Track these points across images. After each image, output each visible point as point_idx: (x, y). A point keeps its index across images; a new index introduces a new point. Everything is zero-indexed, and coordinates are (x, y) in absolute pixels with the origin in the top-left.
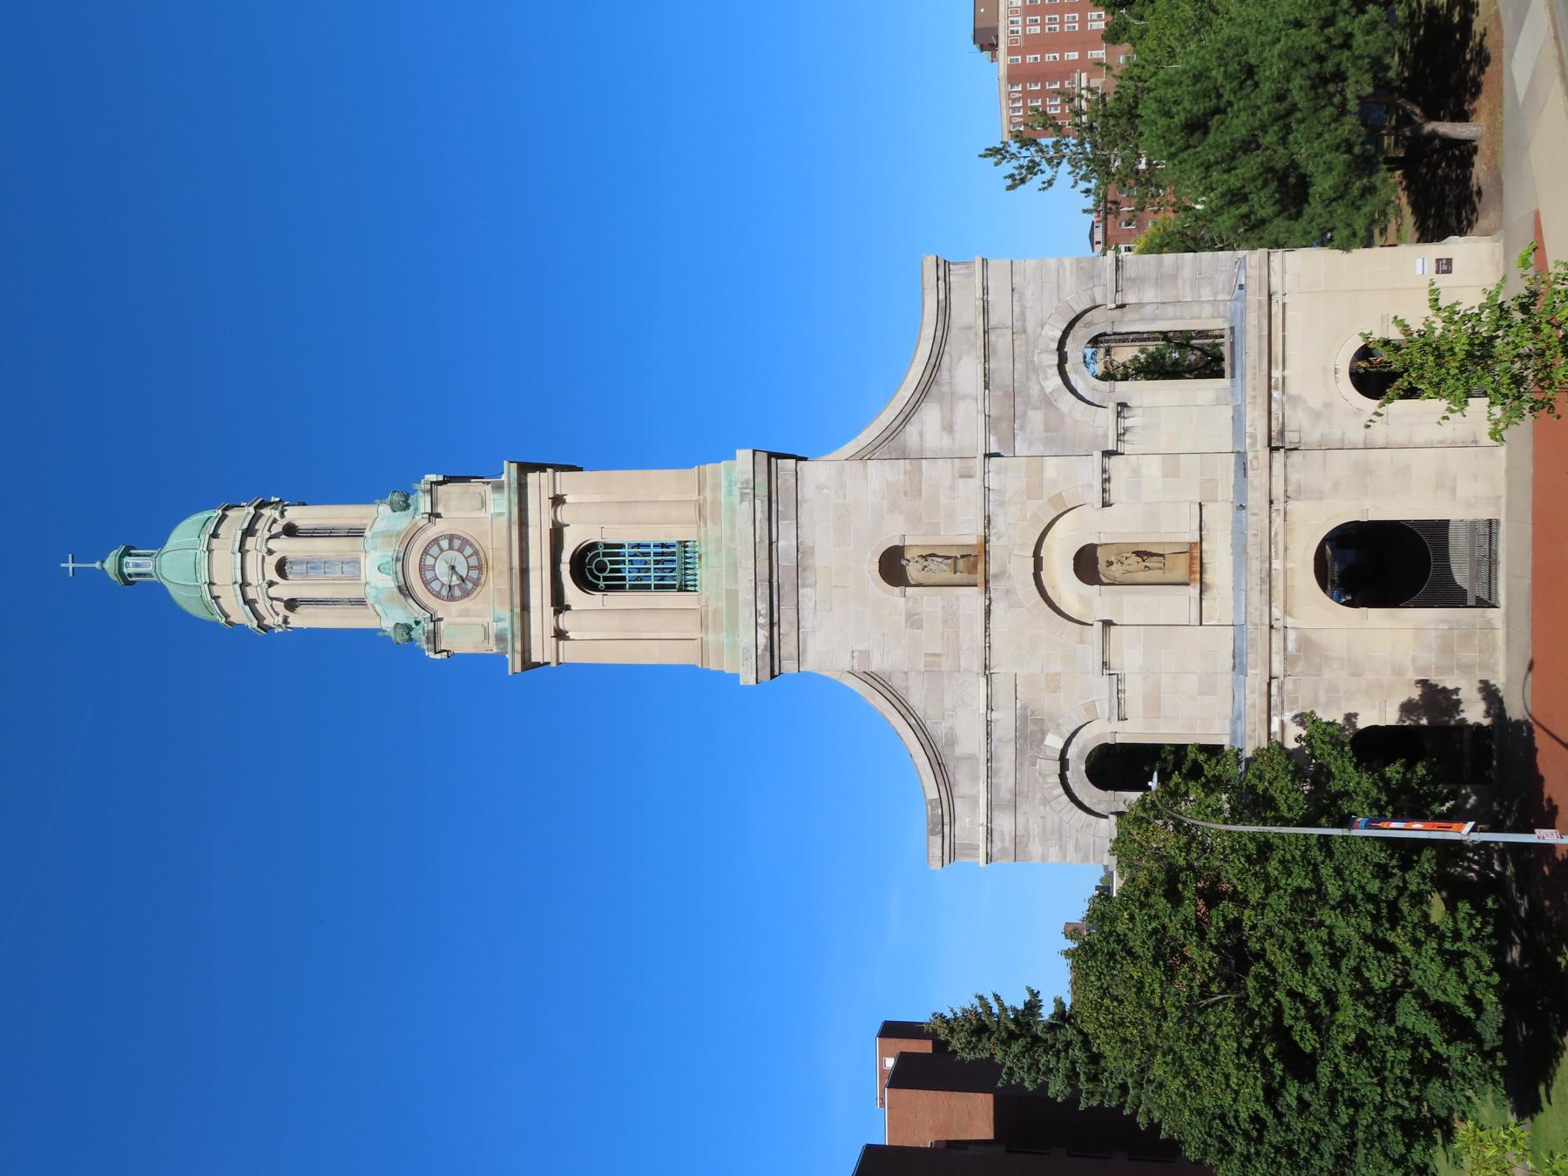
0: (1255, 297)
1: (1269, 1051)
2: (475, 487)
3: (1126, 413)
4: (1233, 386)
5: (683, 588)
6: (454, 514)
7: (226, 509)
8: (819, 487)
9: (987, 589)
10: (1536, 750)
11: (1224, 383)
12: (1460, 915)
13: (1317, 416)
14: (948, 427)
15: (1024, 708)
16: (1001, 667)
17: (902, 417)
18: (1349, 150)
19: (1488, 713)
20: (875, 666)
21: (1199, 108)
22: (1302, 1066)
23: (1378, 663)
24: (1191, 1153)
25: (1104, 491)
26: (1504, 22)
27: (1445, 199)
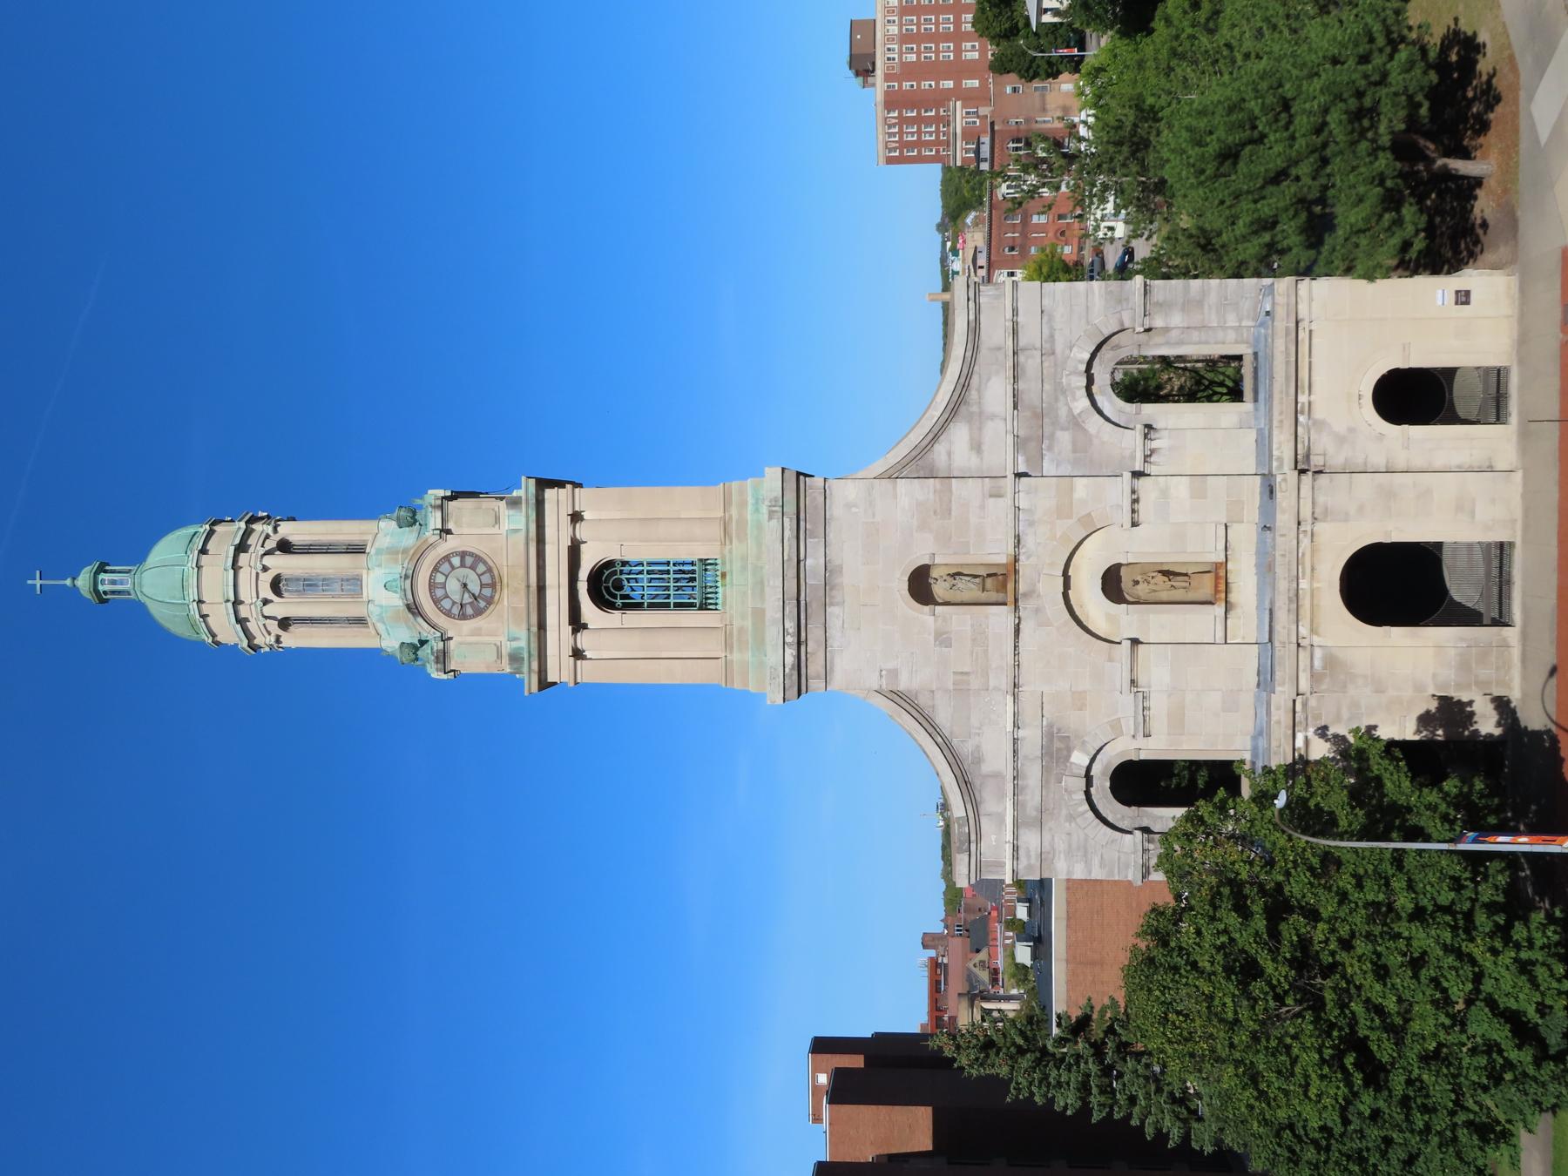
0: (1282, 323)
1: (1349, 1060)
2: (487, 504)
3: (1152, 435)
4: (1256, 409)
5: (703, 607)
6: (466, 531)
7: (214, 524)
8: (849, 506)
9: (1016, 608)
10: (1562, 760)
11: (1246, 407)
12: (1533, 926)
13: (1341, 440)
14: (977, 447)
15: (1051, 726)
16: (1026, 690)
17: (931, 436)
18: (1382, 183)
19: (1499, 724)
20: (903, 685)
21: (1235, 138)
22: (1375, 1075)
23: (1398, 678)
24: (1257, 1165)
25: (1133, 511)
26: (1521, 67)
27: (1446, 235)
